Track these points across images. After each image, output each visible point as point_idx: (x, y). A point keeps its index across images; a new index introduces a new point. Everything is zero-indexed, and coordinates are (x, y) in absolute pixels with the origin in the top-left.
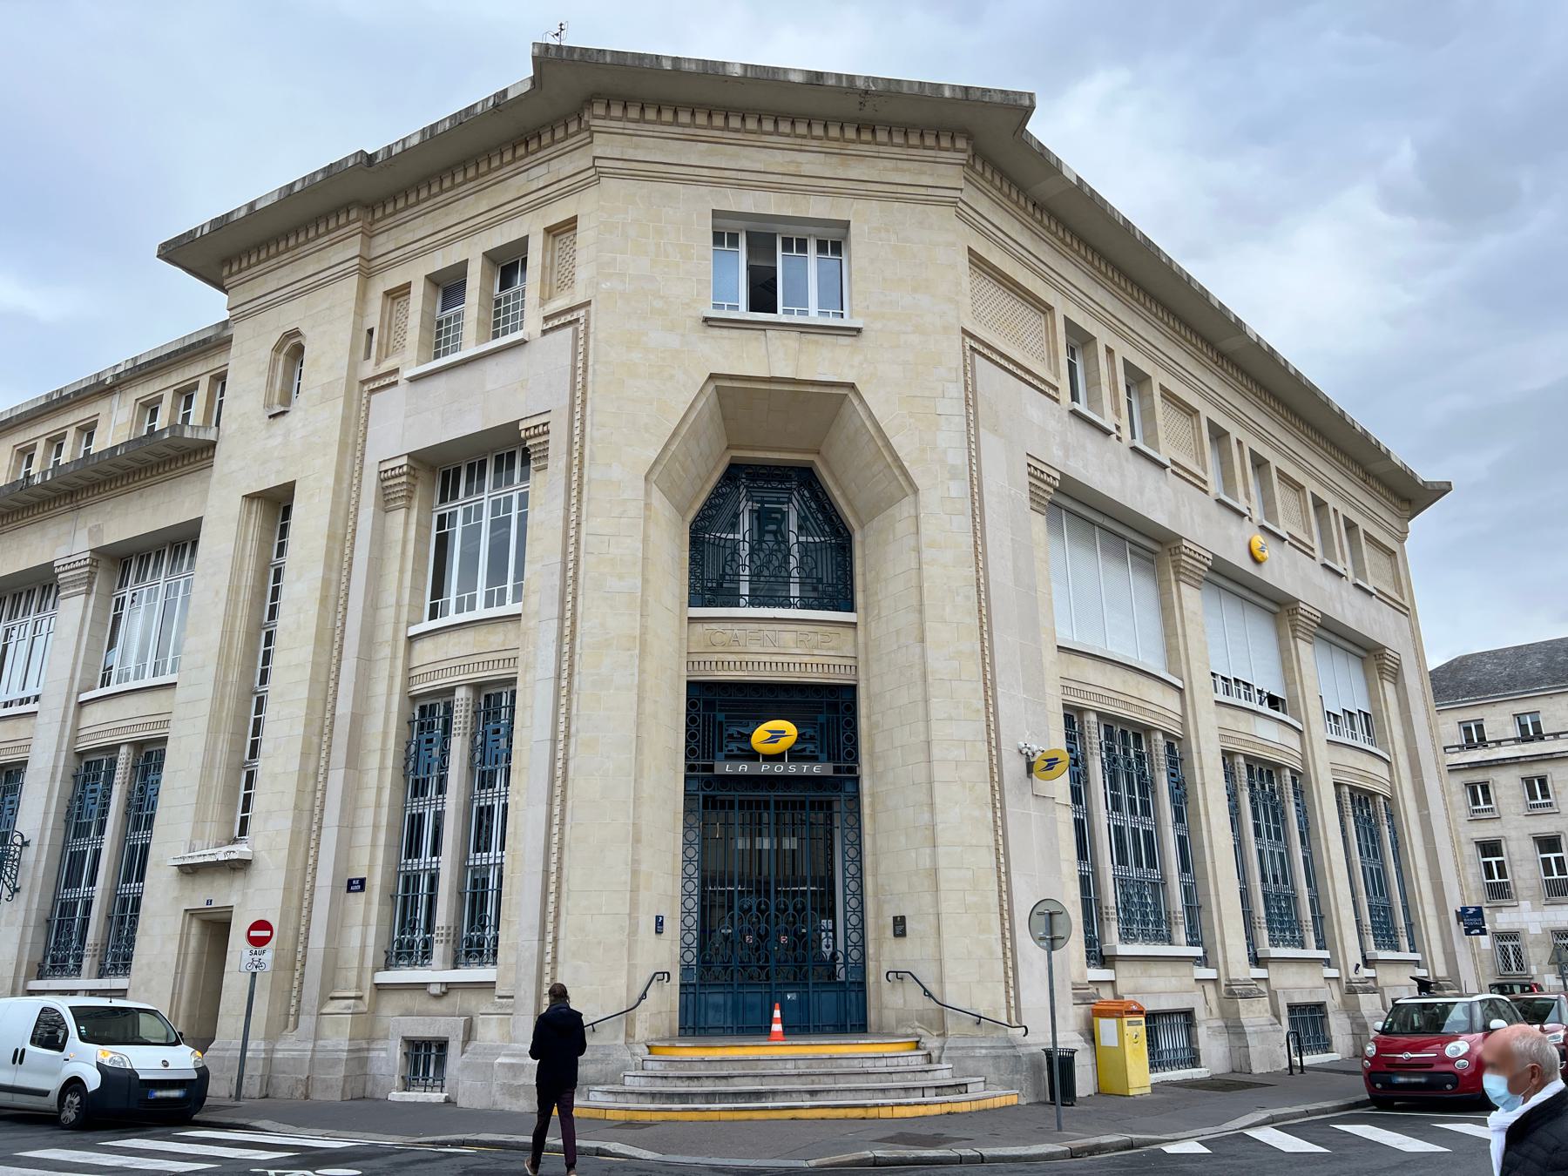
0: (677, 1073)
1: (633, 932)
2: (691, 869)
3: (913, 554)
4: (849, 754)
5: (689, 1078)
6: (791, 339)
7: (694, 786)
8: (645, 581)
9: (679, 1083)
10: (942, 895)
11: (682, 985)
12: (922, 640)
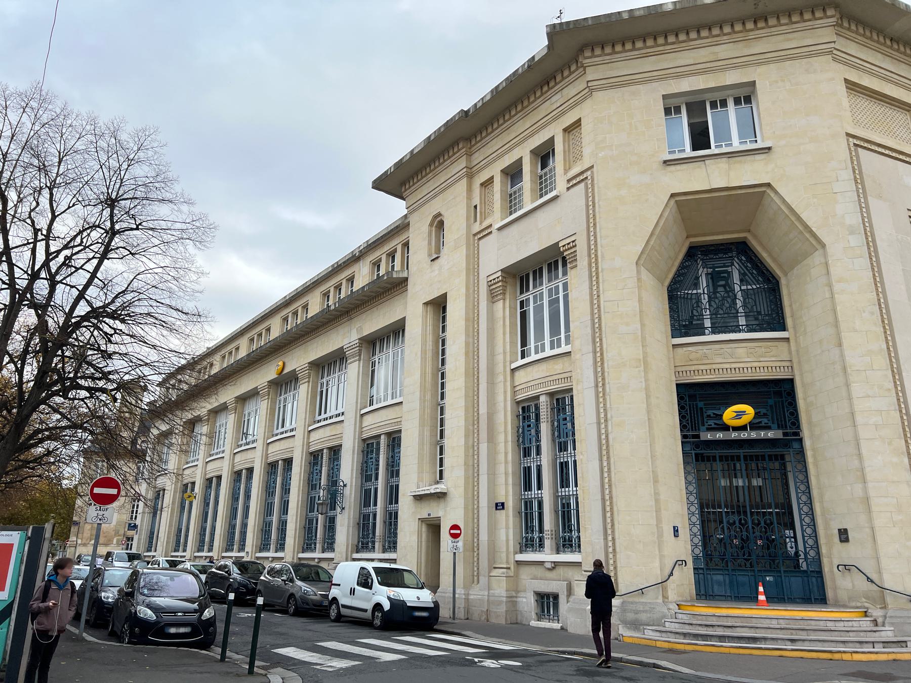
0: (699, 622)
1: (660, 535)
2: (692, 498)
3: (827, 288)
5: (706, 626)
6: (723, 163)
7: (688, 448)
8: (643, 325)
9: (700, 628)
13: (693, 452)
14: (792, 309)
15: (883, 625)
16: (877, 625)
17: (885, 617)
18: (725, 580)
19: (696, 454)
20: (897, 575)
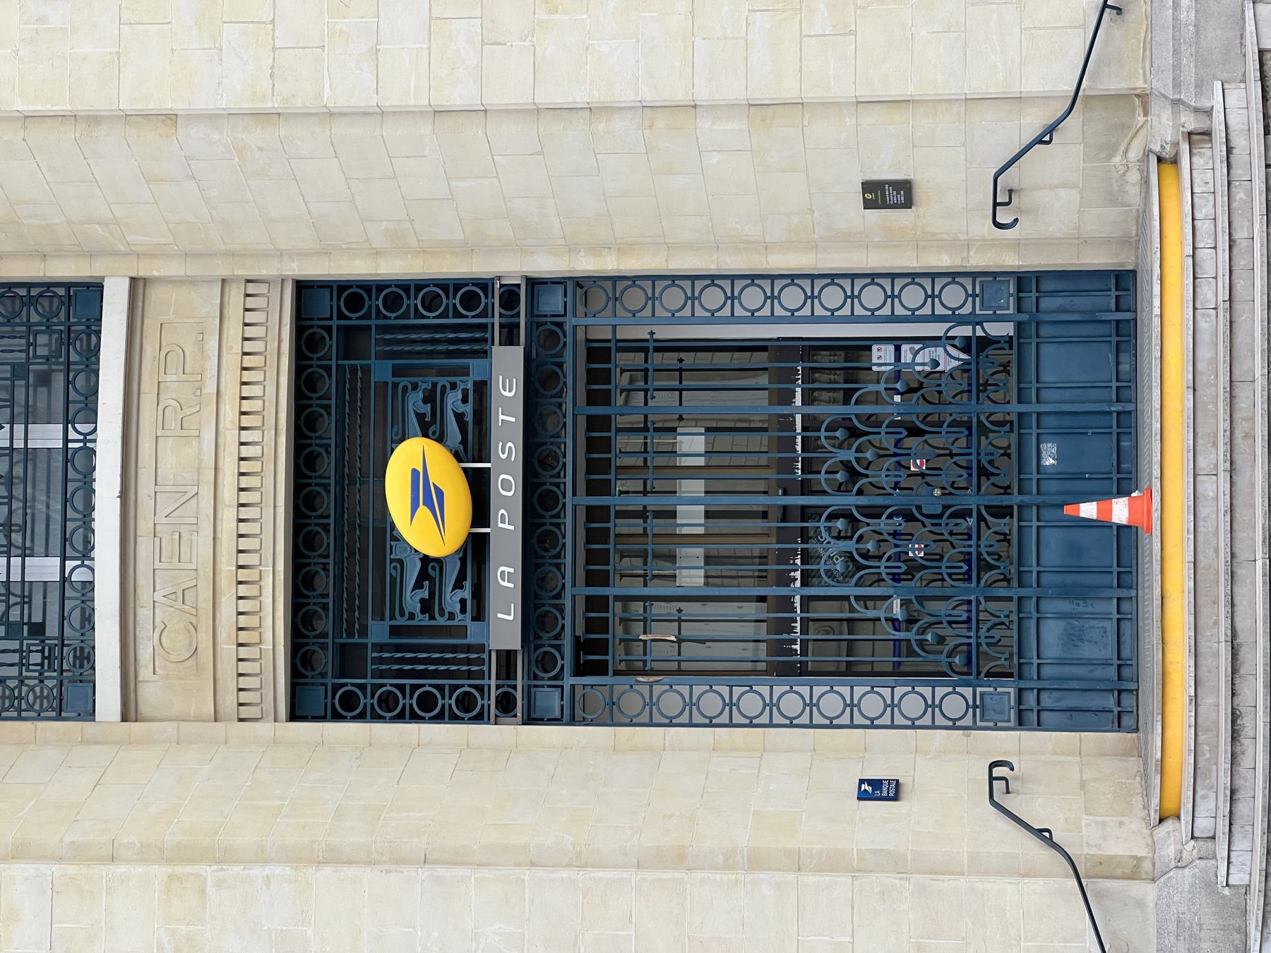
0: (1224, 765)
1: (897, 864)
2: (751, 704)
4: (470, 301)
5: (1235, 736)
7: (550, 700)
9: (1246, 762)
10: (812, 93)
11: (1021, 724)
12: (170, 118)
13: (569, 680)
14: (13, 255)
15: (1209, 113)
16: (1207, 134)
17: (1176, 103)
18: (1062, 616)
19: (579, 671)
20: (1035, 36)
